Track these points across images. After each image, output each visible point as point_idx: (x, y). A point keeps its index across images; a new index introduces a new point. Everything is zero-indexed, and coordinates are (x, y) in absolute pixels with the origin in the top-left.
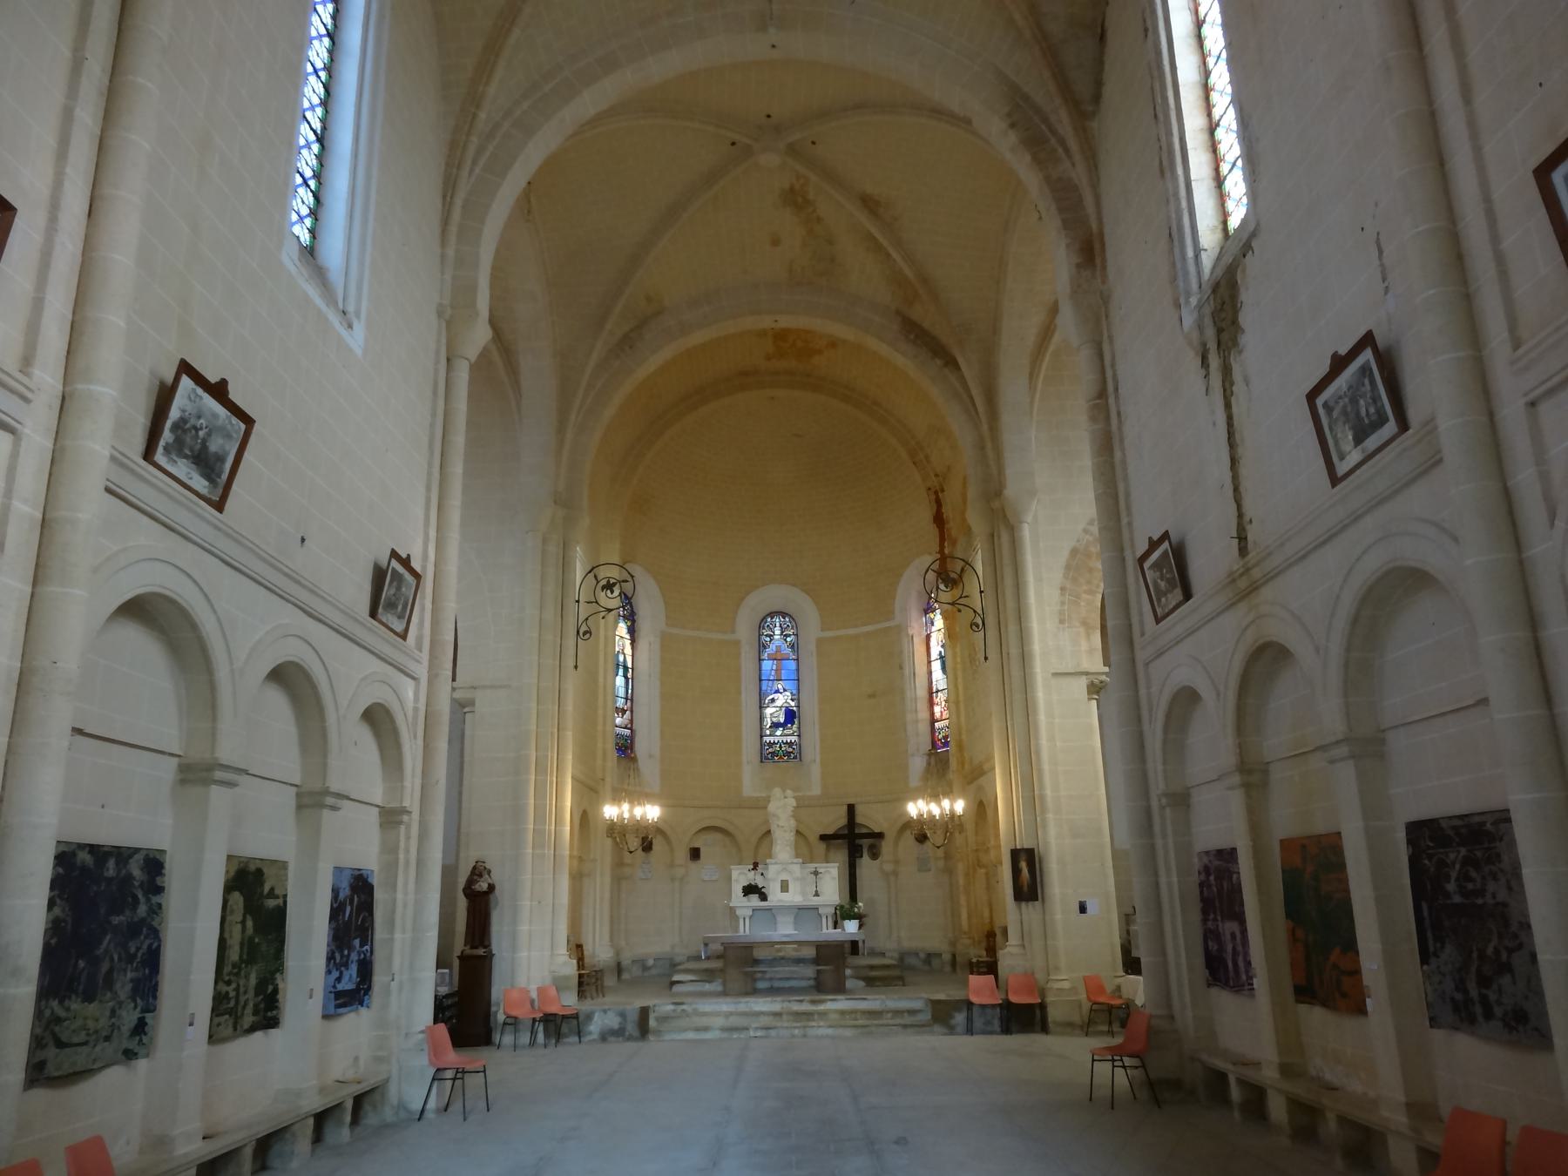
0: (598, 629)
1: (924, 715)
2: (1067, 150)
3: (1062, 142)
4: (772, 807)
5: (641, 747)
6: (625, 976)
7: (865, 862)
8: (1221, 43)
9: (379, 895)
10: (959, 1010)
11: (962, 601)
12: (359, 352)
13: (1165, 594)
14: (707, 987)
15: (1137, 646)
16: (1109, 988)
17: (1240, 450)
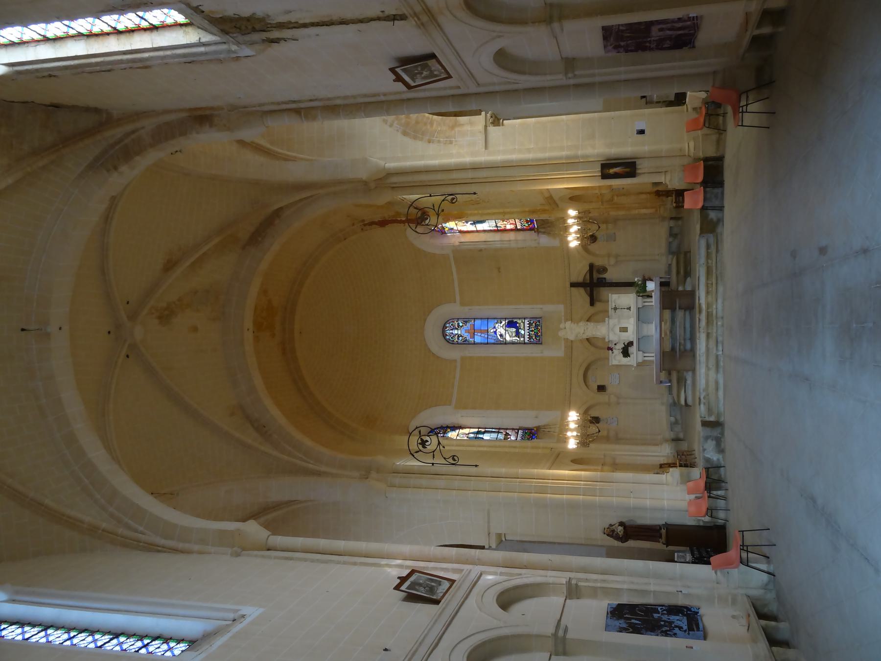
0: (449, 451)
1: (512, 236)
2: (133, 132)
3: (128, 135)
4: (571, 337)
5: (530, 423)
6: (681, 436)
7: (610, 276)
8: (57, 24)
9: (624, 600)
10: (707, 215)
11: (436, 208)
12: (261, 610)
13: (431, 71)
14: (689, 382)
15: (466, 91)
16: (695, 115)
17: (335, 18)
